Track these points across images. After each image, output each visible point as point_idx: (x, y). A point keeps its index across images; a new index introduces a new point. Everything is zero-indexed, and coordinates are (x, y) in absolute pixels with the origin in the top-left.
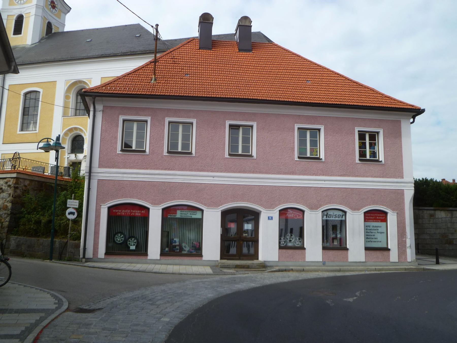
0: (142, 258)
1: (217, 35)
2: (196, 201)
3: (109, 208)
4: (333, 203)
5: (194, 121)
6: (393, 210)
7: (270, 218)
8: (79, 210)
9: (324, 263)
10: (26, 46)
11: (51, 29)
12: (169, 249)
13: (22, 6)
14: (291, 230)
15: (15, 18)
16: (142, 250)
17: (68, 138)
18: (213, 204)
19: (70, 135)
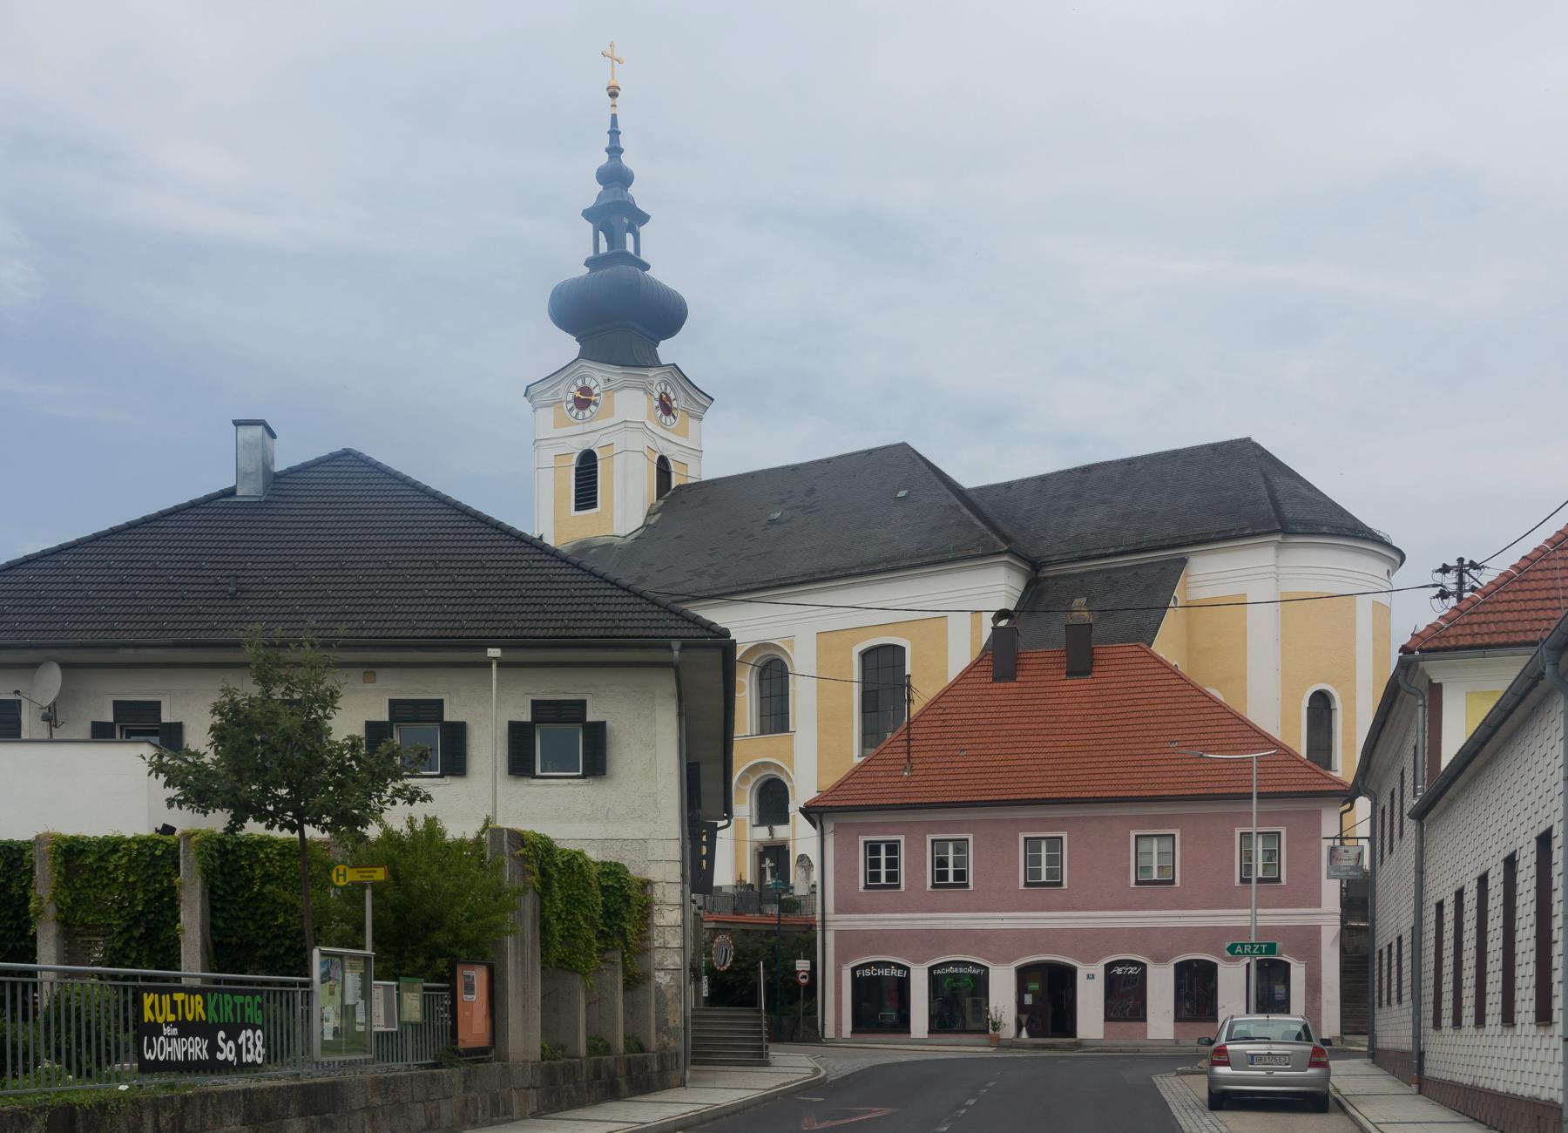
0: (902, 1037)
1: (1123, 460)
2: (978, 955)
3: (854, 970)
4: (1194, 951)
5: (970, 837)
6: (1300, 959)
7: (1090, 977)
8: (812, 972)
9: (1176, 1041)
10: (618, 541)
11: (669, 474)
12: (942, 1021)
13: (587, 427)
14: (1126, 995)
15: (574, 461)
16: (903, 1024)
17: (748, 788)
18: (1003, 959)
19: (753, 780)
